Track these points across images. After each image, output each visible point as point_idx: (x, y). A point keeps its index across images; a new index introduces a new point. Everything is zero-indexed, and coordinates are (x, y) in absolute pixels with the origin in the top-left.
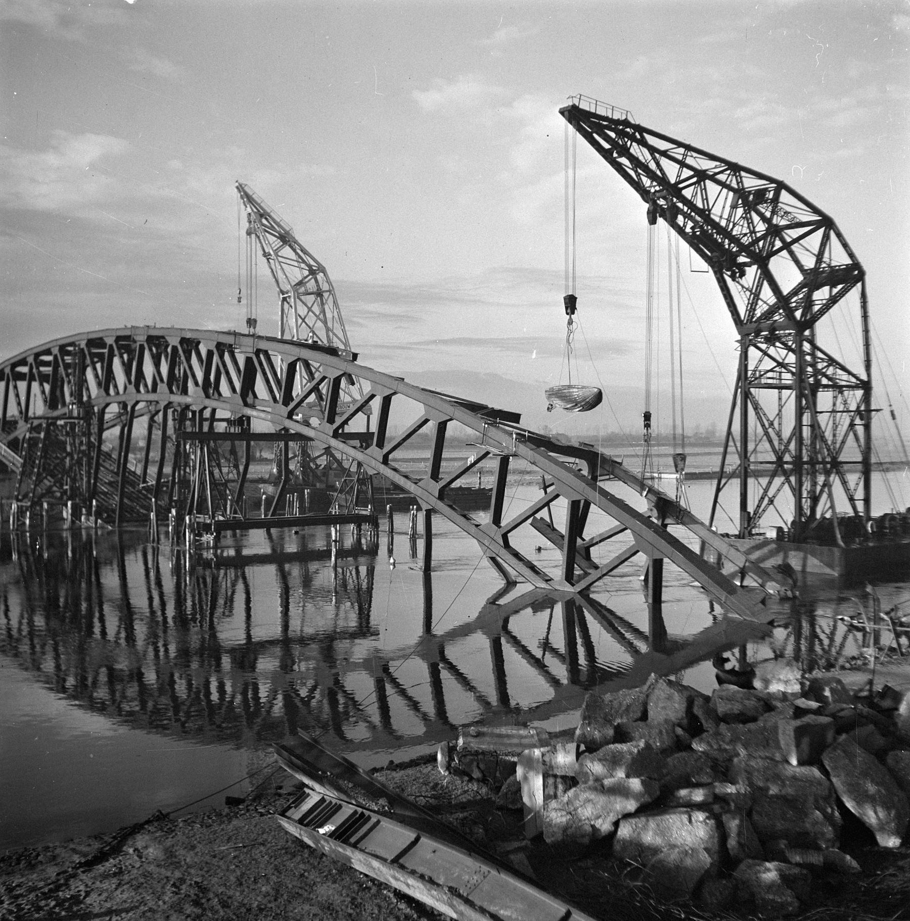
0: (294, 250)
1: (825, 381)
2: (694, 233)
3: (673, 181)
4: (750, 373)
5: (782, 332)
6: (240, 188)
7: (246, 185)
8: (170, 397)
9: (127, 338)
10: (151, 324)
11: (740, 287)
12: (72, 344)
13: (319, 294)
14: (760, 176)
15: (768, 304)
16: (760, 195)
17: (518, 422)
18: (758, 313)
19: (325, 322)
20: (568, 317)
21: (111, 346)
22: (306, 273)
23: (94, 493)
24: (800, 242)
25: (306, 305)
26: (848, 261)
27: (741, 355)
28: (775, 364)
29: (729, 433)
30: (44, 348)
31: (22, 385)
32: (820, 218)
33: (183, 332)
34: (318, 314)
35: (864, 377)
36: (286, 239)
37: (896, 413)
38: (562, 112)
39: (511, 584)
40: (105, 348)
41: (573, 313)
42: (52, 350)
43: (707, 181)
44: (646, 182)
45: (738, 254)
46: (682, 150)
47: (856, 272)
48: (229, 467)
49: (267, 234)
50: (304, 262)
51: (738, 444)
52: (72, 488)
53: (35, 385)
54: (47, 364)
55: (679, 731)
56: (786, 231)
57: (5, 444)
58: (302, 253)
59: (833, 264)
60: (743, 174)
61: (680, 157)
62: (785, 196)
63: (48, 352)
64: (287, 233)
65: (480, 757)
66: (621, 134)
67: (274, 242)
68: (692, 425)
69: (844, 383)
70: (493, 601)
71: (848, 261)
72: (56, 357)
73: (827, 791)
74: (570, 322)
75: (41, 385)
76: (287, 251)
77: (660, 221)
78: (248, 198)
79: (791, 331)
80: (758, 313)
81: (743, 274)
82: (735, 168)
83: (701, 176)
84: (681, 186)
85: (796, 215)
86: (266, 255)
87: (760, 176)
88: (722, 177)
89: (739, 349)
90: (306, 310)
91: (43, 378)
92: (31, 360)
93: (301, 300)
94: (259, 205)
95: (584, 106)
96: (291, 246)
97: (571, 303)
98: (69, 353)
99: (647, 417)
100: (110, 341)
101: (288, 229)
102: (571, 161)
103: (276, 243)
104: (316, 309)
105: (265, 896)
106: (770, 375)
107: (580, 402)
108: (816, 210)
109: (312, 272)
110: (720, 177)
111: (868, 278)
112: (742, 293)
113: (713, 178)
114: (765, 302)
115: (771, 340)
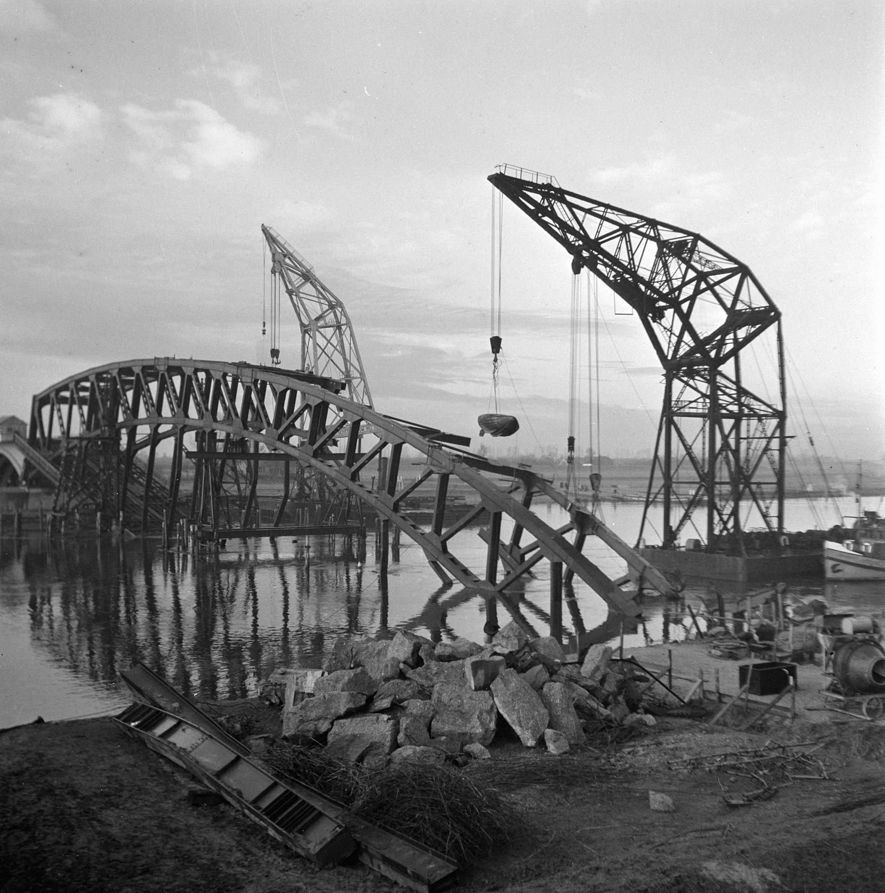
0: (315, 287)
1: (746, 411)
2: (616, 280)
3: (592, 237)
4: (673, 403)
5: (701, 367)
6: (265, 230)
7: (271, 228)
8: (185, 421)
9: (151, 367)
10: (171, 356)
11: (662, 328)
12: (107, 372)
13: (339, 327)
14: (676, 229)
15: (689, 345)
16: (681, 245)
17: (468, 445)
18: (681, 352)
19: (343, 353)
20: (494, 355)
21: (138, 375)
22: (326, 307)
23: (124, 504)
24: (721, 284)
25: (325, 337)
26: (766, 304)
27: (666, 387)
28: (699, 395)
29: (656, 456)
30: (83, 376)
31: (65, 408)
32: (736, 266)
33: (196, 363)
34: (335, 345)
35: (780, 408)
36: (307, 277)
37: (814, 439)
38: (490, 178)
39: (448, 584)
40: (133, 376)
41: (498, 352)
42: (90, 377)
43: (631, 234)
44: (571, 238)
45: (657, 300)
46: (602, 209)
47: (773, 314)
48: (246, 483)
49: (289, 272)
50: (324, 298)
51: (663, 466)
52: (104, 501)
53: (75, 408)
54: (85, 389)
55: (402, 666)
56: (711, 277)
57: (49, 462)
58: (322, 290)
59: (753, 306)
60: (659, 227)
61: (601, 213)
62: (701, 245)
63: (86, 379)
64: (308, 271)
65: (278, 687)
66: (545, 196)
67: (296, 279)
68: (610, 449)
69: (762, 413)
70: (434, 599)
71: (766, 304)
72: (92, 384)
73: (489, 707)
74: (496, 360)
75: (80, 408)
76: (308, 288)
77: (585, 270)
78: (271, 239)
79: (706, 367)
80: (681, 352)
81: (662, 316)
82: (653, 223)
83: (625, 230)
84: (600, 241)
85: (716, 263)
86: (290, 293)
87: (676, 229)
88: (643, 230)
89: (664, 381)
90: (325, 342)
91: (82, 401)
92: (72, 386)
93: (319, 332)
94: (282, 245)
95: (510, 173)
96: (311, 283)
97: (496, 343)
98: (103, 380)
99: (571, 441)
100: (137, 370)
101: (309, 268)
102: (497, 223)
103: (298, 280)
104: (334, 341)
105: (315, 884)
106: (693, 405)
107: (500, 428)
108: (731, 259)
109: (332, 307)
110: (641, 230)
111: (783, 318)
112: (664, 333)
113: (636, 231)
114: (686, 344)
115: (691, 374)
